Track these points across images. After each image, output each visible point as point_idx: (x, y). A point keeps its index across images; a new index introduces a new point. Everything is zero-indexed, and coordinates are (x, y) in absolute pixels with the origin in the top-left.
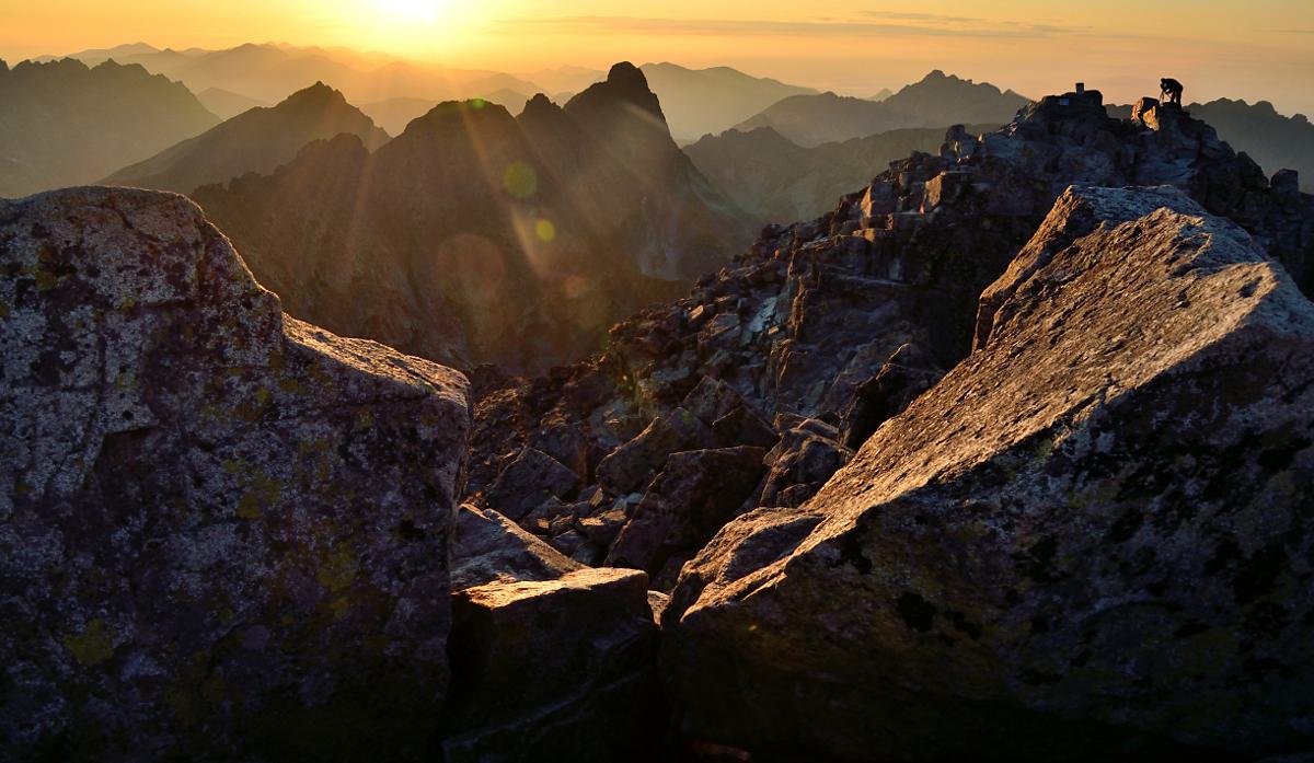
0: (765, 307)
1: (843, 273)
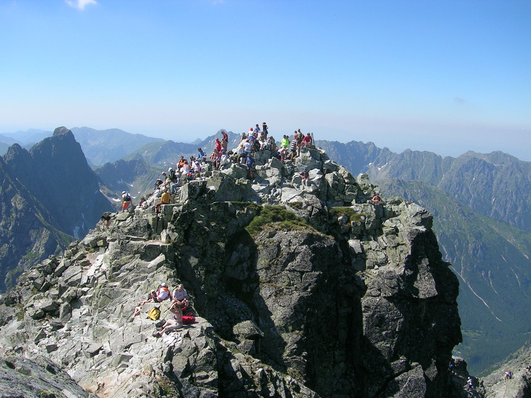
0: (98, 260)
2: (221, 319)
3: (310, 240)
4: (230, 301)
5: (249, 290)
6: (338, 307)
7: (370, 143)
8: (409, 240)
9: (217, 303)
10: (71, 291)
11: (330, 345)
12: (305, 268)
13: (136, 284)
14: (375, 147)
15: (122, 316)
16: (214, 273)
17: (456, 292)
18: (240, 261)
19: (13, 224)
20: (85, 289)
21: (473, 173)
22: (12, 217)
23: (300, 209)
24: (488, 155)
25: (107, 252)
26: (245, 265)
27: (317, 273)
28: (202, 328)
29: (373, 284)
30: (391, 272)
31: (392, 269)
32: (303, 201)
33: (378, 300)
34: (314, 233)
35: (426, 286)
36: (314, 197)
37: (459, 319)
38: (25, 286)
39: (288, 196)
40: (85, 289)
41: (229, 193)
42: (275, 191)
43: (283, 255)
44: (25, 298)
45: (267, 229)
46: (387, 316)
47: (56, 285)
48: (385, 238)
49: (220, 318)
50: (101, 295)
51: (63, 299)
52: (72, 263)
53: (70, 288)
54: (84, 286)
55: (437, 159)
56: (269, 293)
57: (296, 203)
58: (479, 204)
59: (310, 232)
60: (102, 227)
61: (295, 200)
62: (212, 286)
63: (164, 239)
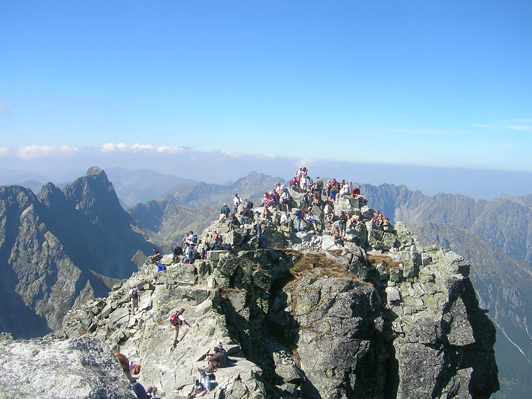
0: (144, 303)
1: (182, 284)
2: (264, 363)
3: (350, 286)
4: (272, 346)
5: (290, 336)
6: (377, 353)
7: (402, 186)
8: (447, 288)
9: (259, 347)
10: (118, 333)
11: (369, 390)
12: (345, 315)
14: (407, 190)
15: (171, 358)
16: (257, 318)
17: (493, 340)
19: (44, 261)
20: (132, 331)
22: (45, 255)
23: (340, 255)
24: (523, 198)
25: (154, 296)
28: (252, 372)
29: (411, 331)
31: (429, 316)
32: (342, 248)
33: (416, 346)
34: (354, 280)
35: (462, 335)
36: (354, 244)
37: (496, 367)
38: (72, 326)
40: (132, 331)
42: (316, 238)
43: (323, 301)
45: (308, 276)
46: (425, 362)
47: (103, 327)
48: (422, 285)
49: (263, 362)
52: (120, 305)
54: (132, 328)
55: (470, 202)
56: (310, 339)
57: (336, 251)
58: (513, 248)
59: (350, 279)
60: (146, 271)
62: (255, 330)
63: (210, 284)
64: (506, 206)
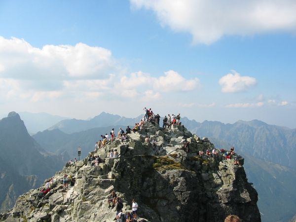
13: (100, 202)
18: (148, 187)
20: (66, 206)
21: (242, 132)
26: (151, 189)
27: (190, 192)
30: (226, 190)
32: (178, 153)
39: (170, 150)
40: (66, 206)
41: (139, 150)
44: (26, 213)
50: (79, 209)
51: (54, 212)
53: (57, 205)
54: (65, 204)
61: (173, 153)
64: (93, 120)
